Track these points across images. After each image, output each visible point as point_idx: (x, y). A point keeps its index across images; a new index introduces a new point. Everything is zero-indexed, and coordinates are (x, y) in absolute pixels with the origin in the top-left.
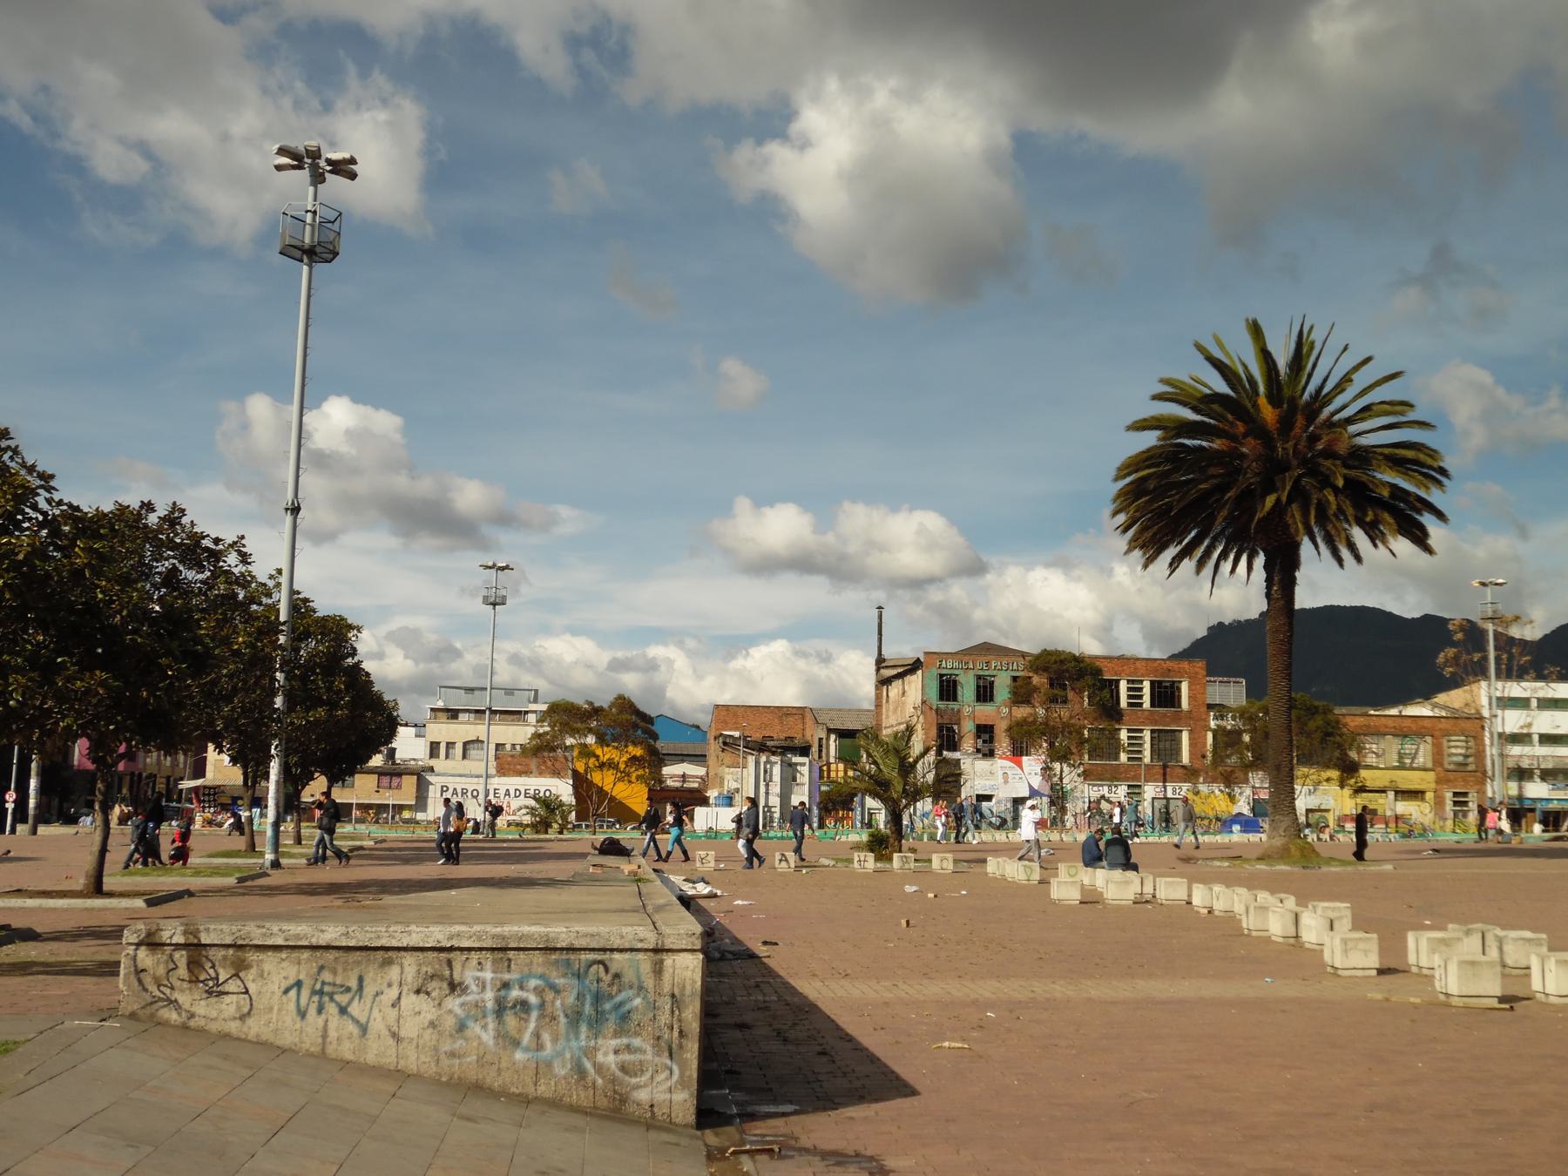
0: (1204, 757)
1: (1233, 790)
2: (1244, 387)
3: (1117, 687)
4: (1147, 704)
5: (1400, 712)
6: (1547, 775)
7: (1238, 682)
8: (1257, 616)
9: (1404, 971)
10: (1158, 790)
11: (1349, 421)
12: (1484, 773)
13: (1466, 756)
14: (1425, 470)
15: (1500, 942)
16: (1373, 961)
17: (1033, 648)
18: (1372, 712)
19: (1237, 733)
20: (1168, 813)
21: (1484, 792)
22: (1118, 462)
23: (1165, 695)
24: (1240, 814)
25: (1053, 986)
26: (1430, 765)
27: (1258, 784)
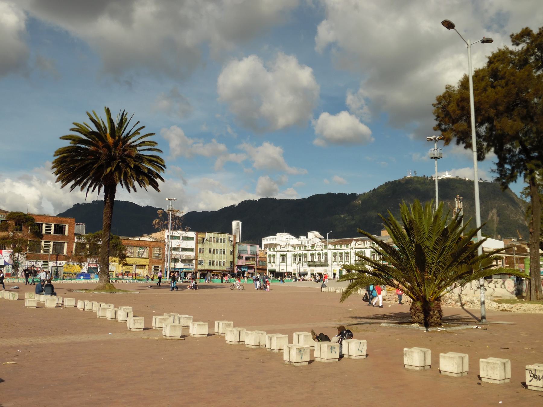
0: (72, 252)
1: (82, 264)
2: (102, 130)
3: (42, 226)
4: (52, 233)
5: (139, 239)
6: (183, 261)
7: (83, 225)
8: (91, 202)
9: (151, 329)
10: (54, 263)
11: (137, 146)
12: (164, 260)
13: (159, 254)
14: (159, 165)
15: (179, 319)
16: (142, 326)
17: (9, 210)
18: (130, 239)
19: (84, 244)
20: (57, 272)
21: (164, 266)
22: (55, 150)
23: (60, 230)
24: (84, 272)
25: (37, 339)
26: (147, 257)
27: (92, 262)
